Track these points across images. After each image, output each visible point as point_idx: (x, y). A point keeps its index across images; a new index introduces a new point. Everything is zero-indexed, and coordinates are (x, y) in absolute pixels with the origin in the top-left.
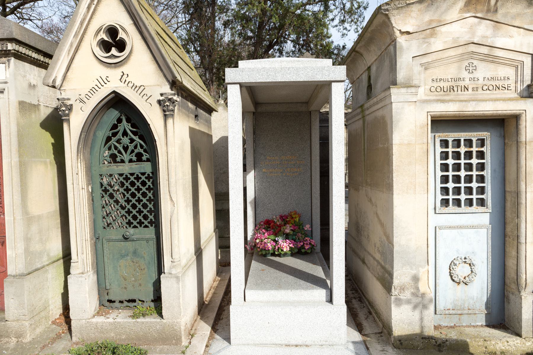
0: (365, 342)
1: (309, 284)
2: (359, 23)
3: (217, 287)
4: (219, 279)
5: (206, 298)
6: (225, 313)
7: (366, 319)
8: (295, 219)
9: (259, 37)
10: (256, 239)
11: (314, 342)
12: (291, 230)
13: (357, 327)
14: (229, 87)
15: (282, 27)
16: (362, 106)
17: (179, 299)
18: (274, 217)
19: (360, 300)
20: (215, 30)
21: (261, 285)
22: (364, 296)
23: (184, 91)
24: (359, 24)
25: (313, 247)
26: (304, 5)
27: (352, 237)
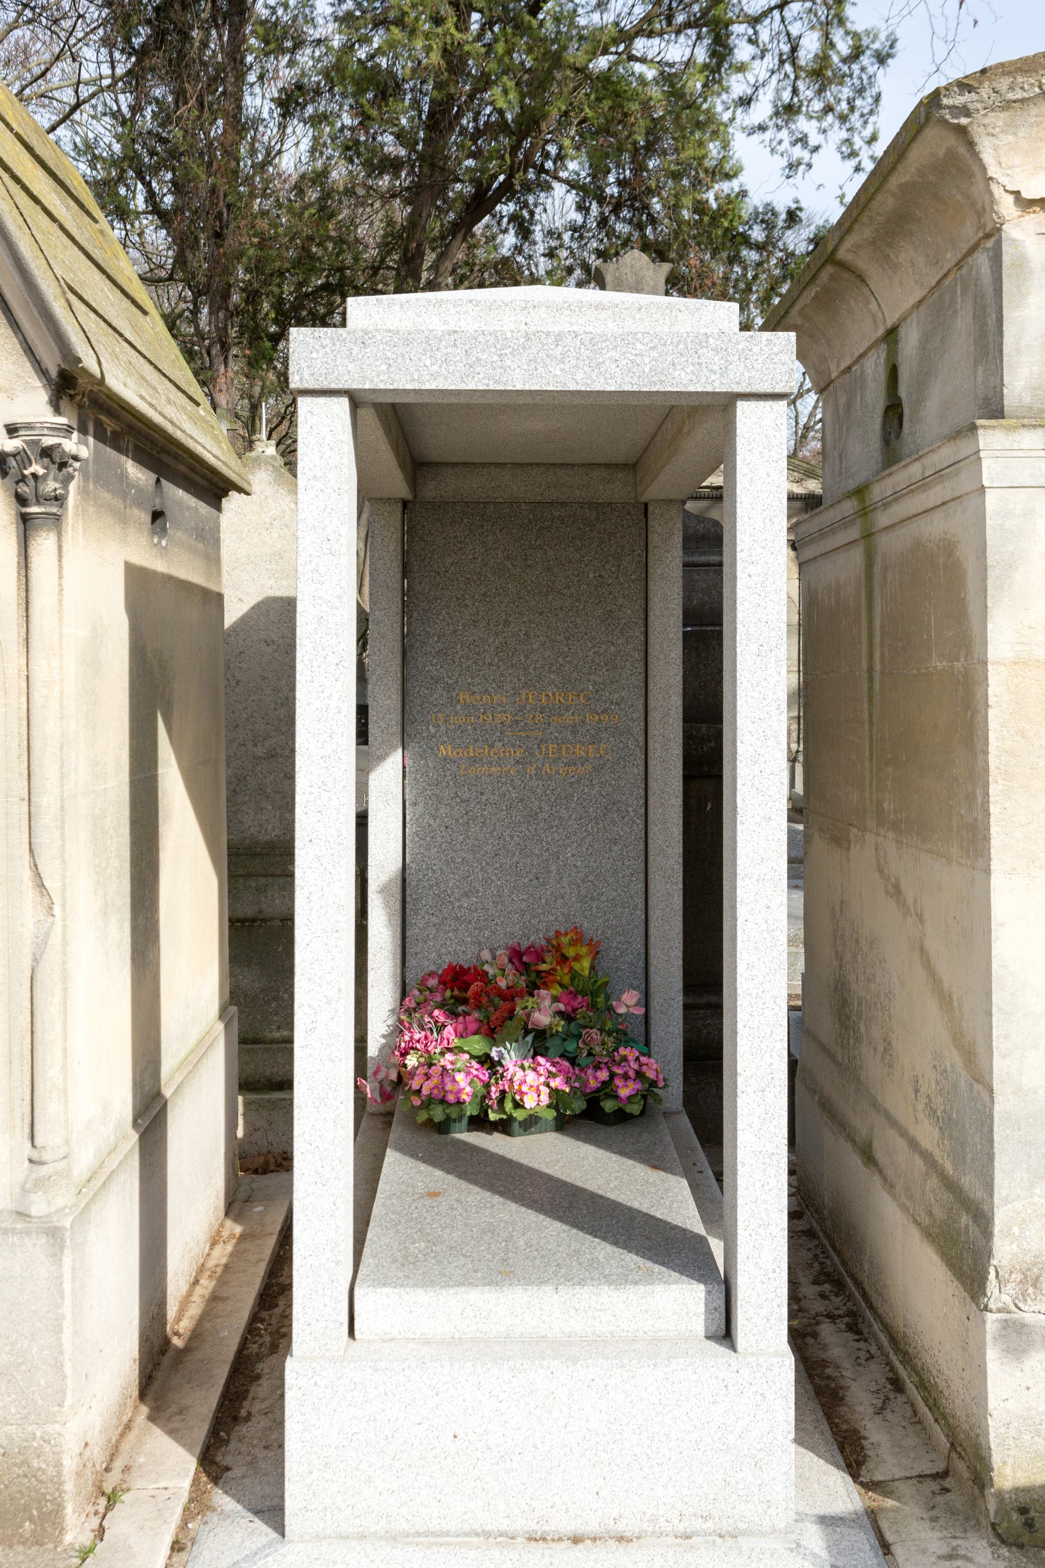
0: (872, 1515)
1: (632, 1259)
2: (855, 119)
3: (226, 1266)
4: (238, 1229)
5: (178, 1319)
6: (261, 1389)
7: (880, 1411)
8: (576, 966)
9: (433, 166)
10: (404, 1054)
11: (653, 1520)
12: (560, 1013)
13: (842, 1449)
14: (303, 403)
15: (529, 124)
16: (860, 492)
17: (59, 1330)
18: (486, 955)
19: (855, 1327)
20: (240, 125)
21: (430, 1264)
22: (871, 1307)
23: (110, 413)
24: (858, 124)
25: (649, 1091)
26: (626, 37)
27: (819, 1042)
